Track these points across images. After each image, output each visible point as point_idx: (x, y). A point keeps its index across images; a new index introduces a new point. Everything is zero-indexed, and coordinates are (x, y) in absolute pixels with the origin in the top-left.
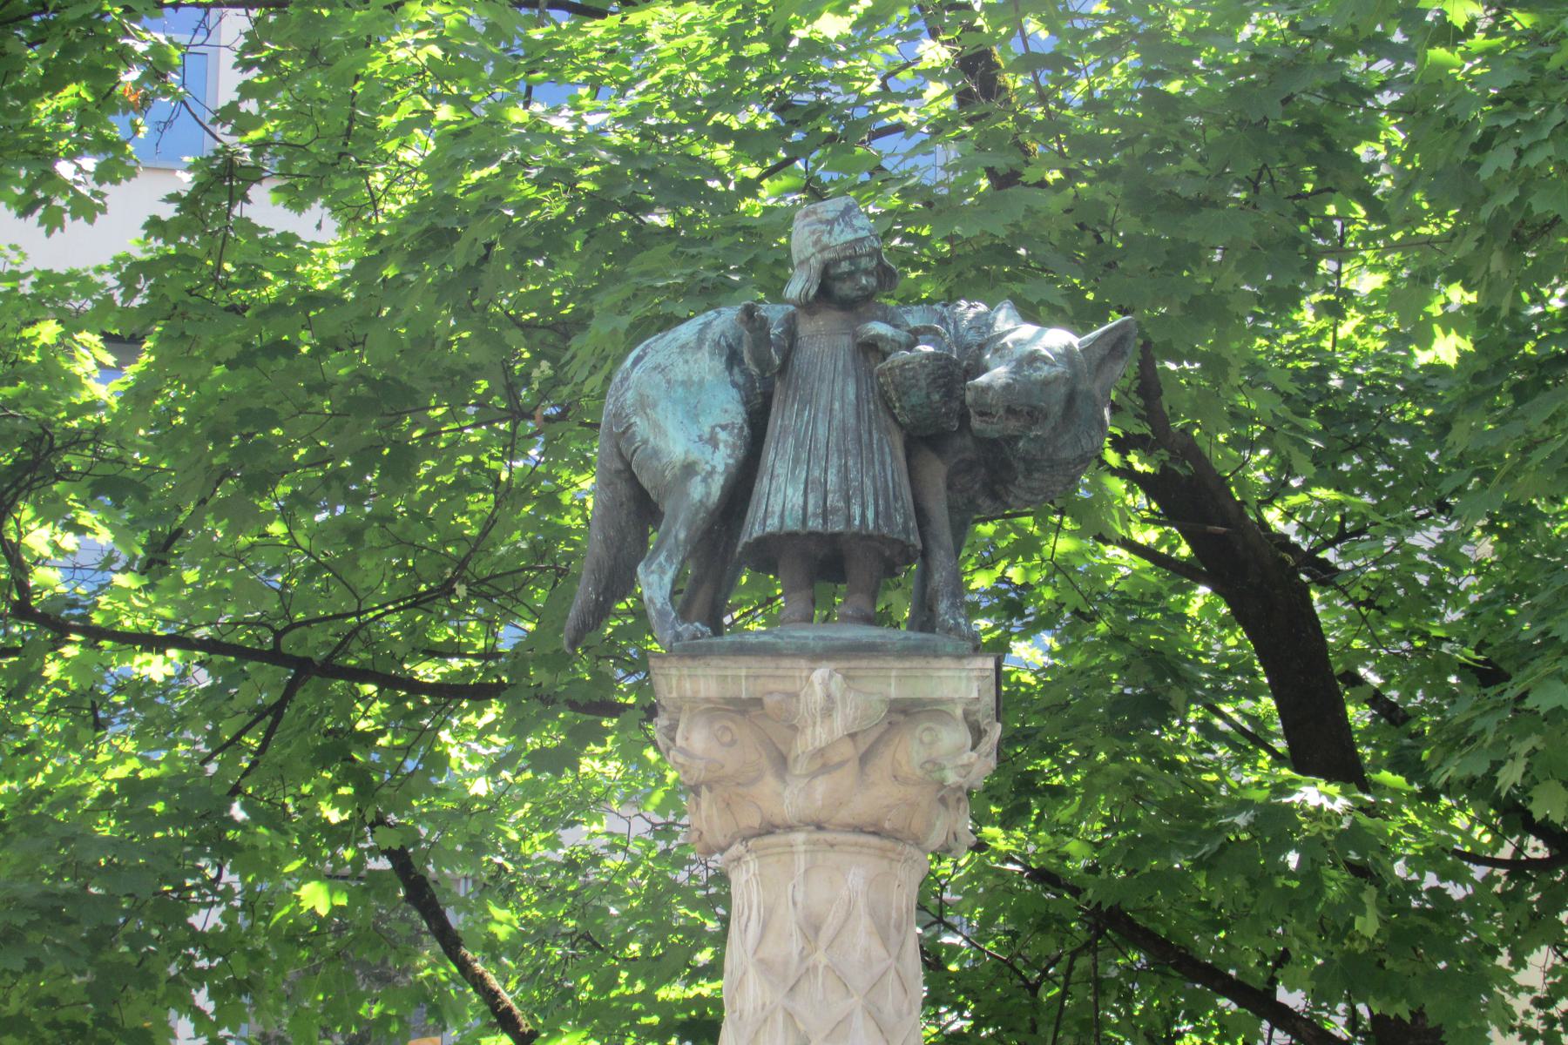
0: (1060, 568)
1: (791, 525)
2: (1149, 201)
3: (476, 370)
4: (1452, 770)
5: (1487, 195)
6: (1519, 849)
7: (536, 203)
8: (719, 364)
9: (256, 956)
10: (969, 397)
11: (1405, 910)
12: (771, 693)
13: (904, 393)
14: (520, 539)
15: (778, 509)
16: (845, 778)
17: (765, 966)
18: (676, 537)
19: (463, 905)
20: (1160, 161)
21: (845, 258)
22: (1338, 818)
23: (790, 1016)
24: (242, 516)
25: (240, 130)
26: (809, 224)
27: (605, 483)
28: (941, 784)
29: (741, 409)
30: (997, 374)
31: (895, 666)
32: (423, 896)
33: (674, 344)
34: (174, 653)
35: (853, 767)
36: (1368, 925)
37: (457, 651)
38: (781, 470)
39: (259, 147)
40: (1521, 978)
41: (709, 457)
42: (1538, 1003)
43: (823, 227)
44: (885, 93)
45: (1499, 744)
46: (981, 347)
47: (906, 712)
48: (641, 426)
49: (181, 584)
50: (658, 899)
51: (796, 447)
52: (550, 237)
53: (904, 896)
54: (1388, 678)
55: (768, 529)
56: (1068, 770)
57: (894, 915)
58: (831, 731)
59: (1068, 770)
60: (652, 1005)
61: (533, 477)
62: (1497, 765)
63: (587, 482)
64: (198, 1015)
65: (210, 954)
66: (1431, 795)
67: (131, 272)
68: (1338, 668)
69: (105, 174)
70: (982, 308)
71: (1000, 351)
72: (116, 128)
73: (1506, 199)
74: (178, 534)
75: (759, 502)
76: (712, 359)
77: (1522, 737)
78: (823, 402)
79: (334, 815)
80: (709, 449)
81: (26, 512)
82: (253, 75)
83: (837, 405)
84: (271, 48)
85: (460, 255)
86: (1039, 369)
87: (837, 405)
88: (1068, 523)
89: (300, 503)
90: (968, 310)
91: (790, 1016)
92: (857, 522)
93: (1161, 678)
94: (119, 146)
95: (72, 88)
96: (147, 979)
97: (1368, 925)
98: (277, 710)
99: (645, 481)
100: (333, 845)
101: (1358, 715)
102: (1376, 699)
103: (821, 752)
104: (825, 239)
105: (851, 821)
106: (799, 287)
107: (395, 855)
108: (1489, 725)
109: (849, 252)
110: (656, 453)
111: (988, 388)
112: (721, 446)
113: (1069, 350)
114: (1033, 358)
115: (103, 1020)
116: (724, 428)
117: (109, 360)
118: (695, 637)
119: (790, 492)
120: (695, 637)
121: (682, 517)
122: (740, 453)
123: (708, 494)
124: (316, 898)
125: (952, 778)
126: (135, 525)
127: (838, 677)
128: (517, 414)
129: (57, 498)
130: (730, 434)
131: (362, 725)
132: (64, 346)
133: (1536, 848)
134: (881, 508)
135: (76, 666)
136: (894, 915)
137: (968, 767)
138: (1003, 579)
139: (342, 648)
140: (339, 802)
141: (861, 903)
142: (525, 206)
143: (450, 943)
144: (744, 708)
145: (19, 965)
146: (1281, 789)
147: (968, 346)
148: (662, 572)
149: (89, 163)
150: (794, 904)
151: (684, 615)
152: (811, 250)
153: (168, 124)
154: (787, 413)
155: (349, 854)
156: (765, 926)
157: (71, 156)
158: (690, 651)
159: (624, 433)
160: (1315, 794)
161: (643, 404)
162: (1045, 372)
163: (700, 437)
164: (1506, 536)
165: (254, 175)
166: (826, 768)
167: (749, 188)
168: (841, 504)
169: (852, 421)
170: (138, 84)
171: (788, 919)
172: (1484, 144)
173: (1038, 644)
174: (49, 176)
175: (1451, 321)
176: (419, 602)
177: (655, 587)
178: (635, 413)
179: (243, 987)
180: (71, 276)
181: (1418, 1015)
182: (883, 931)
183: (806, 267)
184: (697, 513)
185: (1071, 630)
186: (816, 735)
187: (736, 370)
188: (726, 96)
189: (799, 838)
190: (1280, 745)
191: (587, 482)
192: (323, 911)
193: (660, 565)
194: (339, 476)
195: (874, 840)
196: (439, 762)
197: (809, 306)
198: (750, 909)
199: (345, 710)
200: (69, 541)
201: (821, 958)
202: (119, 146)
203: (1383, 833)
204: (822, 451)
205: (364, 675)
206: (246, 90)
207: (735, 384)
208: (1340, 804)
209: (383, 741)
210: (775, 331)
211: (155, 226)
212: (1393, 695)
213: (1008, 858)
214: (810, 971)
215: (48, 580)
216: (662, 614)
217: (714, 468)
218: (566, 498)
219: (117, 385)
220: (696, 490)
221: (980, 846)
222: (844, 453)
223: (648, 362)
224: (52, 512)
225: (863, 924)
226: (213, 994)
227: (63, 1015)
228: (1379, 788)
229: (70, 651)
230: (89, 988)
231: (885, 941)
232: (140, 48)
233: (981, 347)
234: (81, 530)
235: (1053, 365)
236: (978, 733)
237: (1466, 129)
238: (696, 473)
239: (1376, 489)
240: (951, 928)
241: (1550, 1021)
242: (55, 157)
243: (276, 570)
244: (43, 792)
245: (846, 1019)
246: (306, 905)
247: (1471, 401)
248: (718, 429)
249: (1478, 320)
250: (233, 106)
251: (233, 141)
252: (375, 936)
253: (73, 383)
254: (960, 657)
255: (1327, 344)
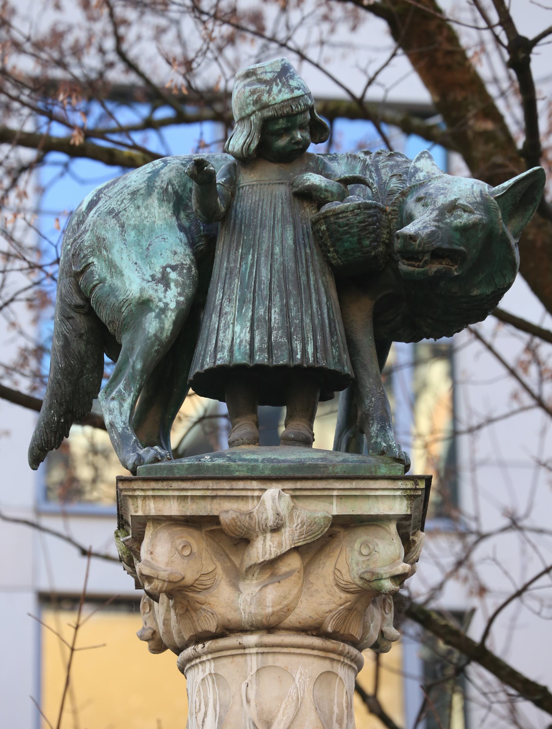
1: (240, 358)
10: (398, 244)
12: (227, 512)
13: (339, 240)
15: (227, 344)
18: (133, 367)
21: (282, 117)
26: (249, 85)
29: (188, 251)
33: (126, 191)
41: (161, 295)
43: (263, 87)
46: (404, 194)
51: (242, 289)
55: (219, 363)
57: (336, 710)
58: (280, 545)
75: (209, 336)
76: (160, 206)
78: (265, 247)
80: (161, 287)
83: (277, 250)
86: (460, 217)
87: (277, 250)
92: (299, 356)
99: (104, 315)
104: (265, 98)
105: (298, 625)
106: (241, 142)
109: (286, 110)
110: (113, 290)
111: (412, 238)
112: (172, 285)
116: (174, 268)
118: (156, 460)
119: (238, 329)
120: (156, 460)
121: (138, 349)
122: (189, 291)
123: (162, 329)
127: (287, 495)
130: (180, 275)
134: (319, 343)
136: (336, 710)
147: (392, 193)
148: (121, 399)
150: (248, 701)
152: (251, 108)
154: (232, 257)
159: (82, 272)
162: (464, 219)
163: (153, 277)
168: (284, 340)
169: (291, 265)
177: (116, 412)
178: (93, 254)
183: (246, 123)
184: (152, 345)
187: (182, 215)
193: (120, 392)
195: (317, 641)
198: (206, 705)
204: (266, 292)
207: (182, 228)
210: (220, 180)
217: (166, 304)
222: (287, 295)
233: (404, 194)
235: (471, 212)
238: (151, 310)
248: (168, 270)
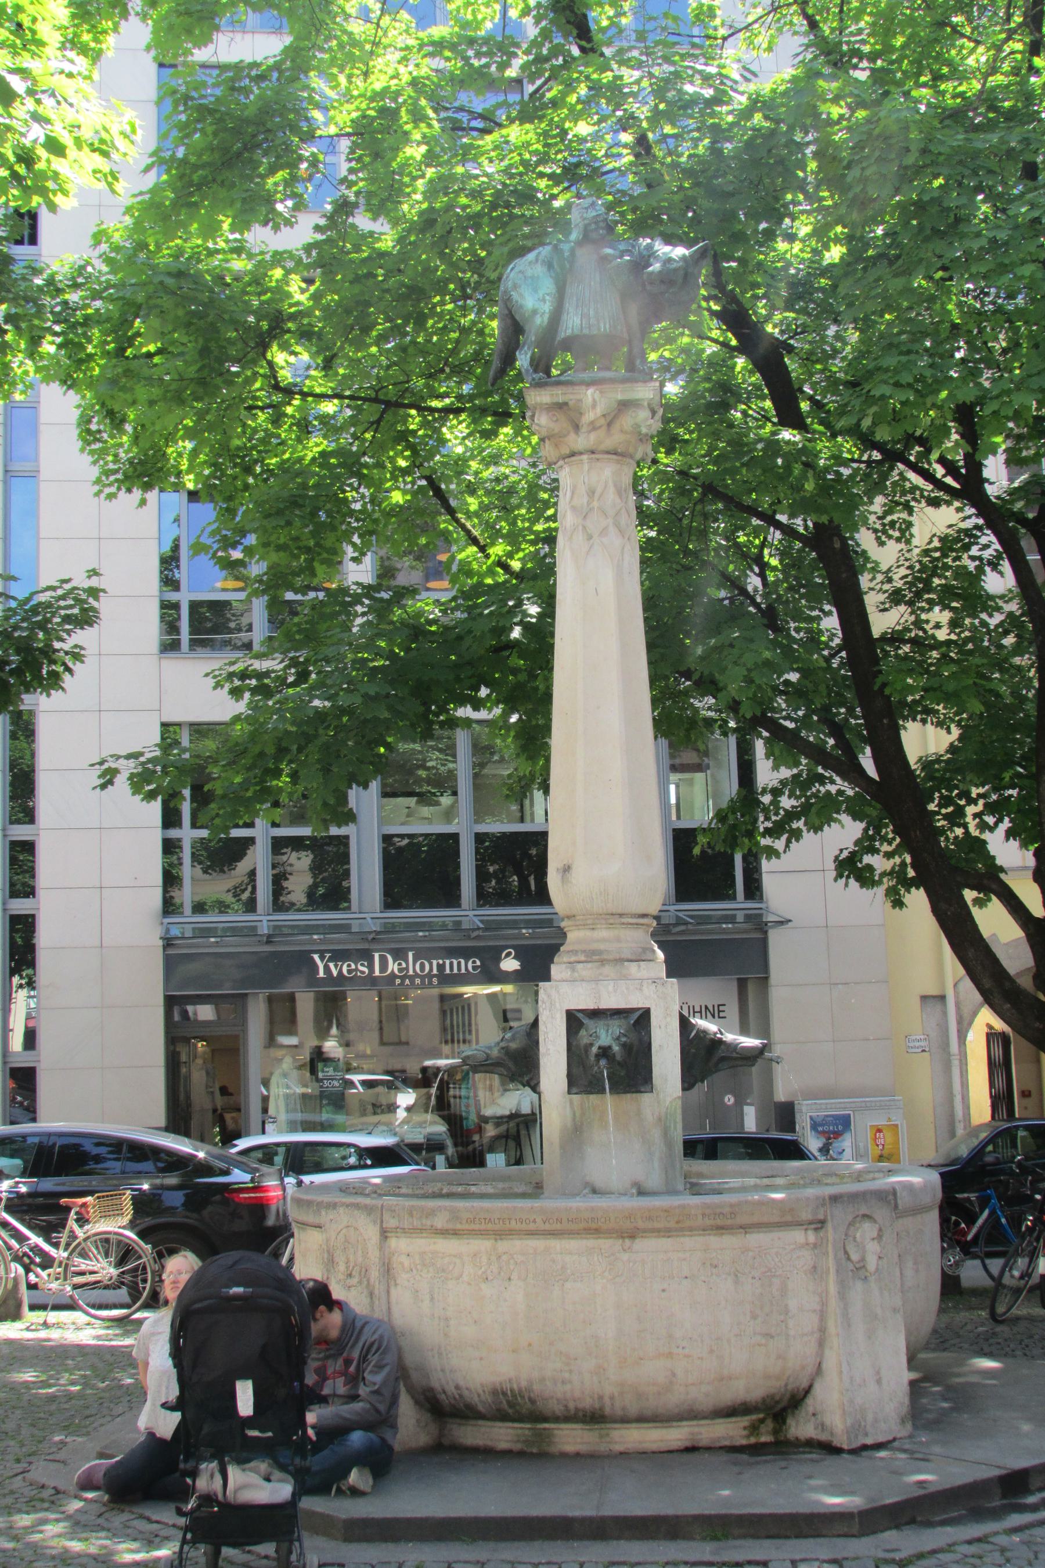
0: (685, 351)
1: (576, 332)
2: (715, 193)
3: (447, 281)
4: (841, 424)
5: (850, 188)
6: (870, 456)
7: (469, 206)
8: (545, 269)
9: (376, 521)
11: (825, 479)
14: (471, 349)
16: (602, 433)
17: (574, 509)
19: (456, 498)
20: (717, 178)
22: (796, 443)
23: (584, 527)
24: (360, 344)
25: (349, 187)
27: (502, 320)
28: (640, 433)
30: (656, 267)
31: (620, 387)
32: (439, 494)
34: (336, 401)
35: (605, 428)
36: (809, 486)
37: (446, 395)
38: (571, 310)
39: (358, 194)
40: (872, 508)
42: (879, 518)
44: (606, 156)
45: (862, 410)
47: (625, 405)
48: (515, 295)
49: (337, 374)
50: (534, 488)
52: (475, 220)
53: (627, 480)
54: (815, 391)
56: (691, 432)
59: (691, 432)
60: (532, 532)
61: (474, 323)
62: (860, 420)
63: (494, 324)
64: (354, 545)
65: (358, 520)
66: (834, 436)
67: (308, 248)
68: (796, 387)
69: (296, 208)
70: (649, 241)
71: (657, 258)
72: (299, 189)
73: (857, 190)
74: (334, 356)
77: (870, 407)
79: (402, 463)
81: (275, 348)
82: (353, 164)
84: (359, 152)
85: (439, 230)
88: (687, 332)
89: (382, 338)
90: (645, 242)
91: (584, 527)
93: (725, 393)
94: (301, 196)
95: (281, 173)
96: (333, 528)
97: (809, 486)
98: (378, 422)
99: (517, 318)
100: (403, 476)
101: (804, 406)
102: (811, 399)
103: (592, 423)
107: (428, 478)
108: (857, 403)
110: (521, 307)
111: (652, 273)
113: (684, 256)
114: (670, 260)
115: (317, 544)
117: (304, 285)
124: (397, 497)
125: (644, 430)
126: (318, 353)
128: (466, 297)
129: (287, 342)
131: (412, 427)
132: (285, 280)
133: (876, 455)
135: (299, 409)
137: (650, 426)
138: (661, 357)
139: (402, 396)
140: (405, 458)
141: (611, 484)
142: (464, 207)
143: (451, 512)
144: (561, 406)
145: (282, 523)
146: (774, 433)
149: (290, 203)
151: (536, 371)
153: (320, 186)
155: (409, 479)
156: (573, 493)
157: (282, 201)
158: (538, 385)
160: (787, 435)
161: (515, 286)
162: (674, 265)
164: (861, 331)
165: (356, 205)
166: (594, 429)
167: (554, 197)
170: (307, 169)
171: (582, 490)
172: (849, 166)
173: (677, 384)
174: (273, 210)
175: (837, 240)
176: (431, 376)
179: (371, 533)
180: (285, 252)
181: (831, 521)
182: (619, 492)
185: (690, 376)
186: (589, 416)
188: (544, 159)
189: (585, 457)
190: (775, 420)
191: (494, 324)
192: (401, 502)
194: (397, 326)
196: (442, 442)
197: (579, 243)
199: (405, 422)
200: (292, 359)
201: (595, 504)
202: (301, 196)
203: (815, 448)
205: (411, 406)
206: (351, 171)
208: (798, 438)
209: (421, 433)
210: (567, 254)
211: (317, 228)
212: (818, 398)
213: (667, 466)
214: (591, 509)
215: (286, 376)
216: (527, 371)
218: (487, 331)
219: (307, 295)
220: (538, 320)
221: (655, 461)
223: (516, 270)
224: (285, 347)
225: (611, 490)
226: (360, 536)
227: (301, 544)
228: (814, 432)
229: (296, 402)
230: (311, 532)
231: (621, 497)
232: (307, 154)
234: (295, 354)
236: (654, 413)
237: (841, 160)
239: (809, 315)
240: (648, 498)
241: (884, 525)
242: (275, 202)
243: (373, 367)
244: (289, 459)
245: (606, 528)
246: (394, 501)
247: (846, 275)
249: (849, 239)
250: (346, 177)
251: (346, 192)
252: (421, 512)
253: (289, 295)
254: (645, 382)
255: (788, 256)
